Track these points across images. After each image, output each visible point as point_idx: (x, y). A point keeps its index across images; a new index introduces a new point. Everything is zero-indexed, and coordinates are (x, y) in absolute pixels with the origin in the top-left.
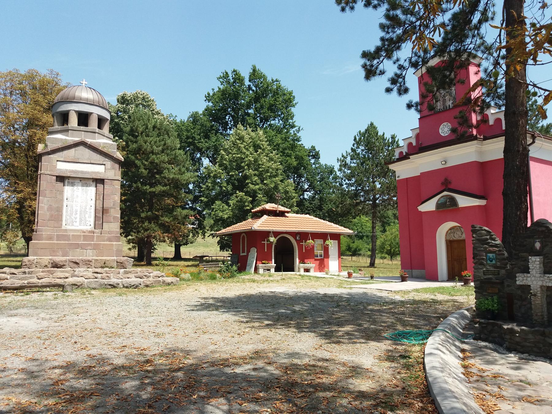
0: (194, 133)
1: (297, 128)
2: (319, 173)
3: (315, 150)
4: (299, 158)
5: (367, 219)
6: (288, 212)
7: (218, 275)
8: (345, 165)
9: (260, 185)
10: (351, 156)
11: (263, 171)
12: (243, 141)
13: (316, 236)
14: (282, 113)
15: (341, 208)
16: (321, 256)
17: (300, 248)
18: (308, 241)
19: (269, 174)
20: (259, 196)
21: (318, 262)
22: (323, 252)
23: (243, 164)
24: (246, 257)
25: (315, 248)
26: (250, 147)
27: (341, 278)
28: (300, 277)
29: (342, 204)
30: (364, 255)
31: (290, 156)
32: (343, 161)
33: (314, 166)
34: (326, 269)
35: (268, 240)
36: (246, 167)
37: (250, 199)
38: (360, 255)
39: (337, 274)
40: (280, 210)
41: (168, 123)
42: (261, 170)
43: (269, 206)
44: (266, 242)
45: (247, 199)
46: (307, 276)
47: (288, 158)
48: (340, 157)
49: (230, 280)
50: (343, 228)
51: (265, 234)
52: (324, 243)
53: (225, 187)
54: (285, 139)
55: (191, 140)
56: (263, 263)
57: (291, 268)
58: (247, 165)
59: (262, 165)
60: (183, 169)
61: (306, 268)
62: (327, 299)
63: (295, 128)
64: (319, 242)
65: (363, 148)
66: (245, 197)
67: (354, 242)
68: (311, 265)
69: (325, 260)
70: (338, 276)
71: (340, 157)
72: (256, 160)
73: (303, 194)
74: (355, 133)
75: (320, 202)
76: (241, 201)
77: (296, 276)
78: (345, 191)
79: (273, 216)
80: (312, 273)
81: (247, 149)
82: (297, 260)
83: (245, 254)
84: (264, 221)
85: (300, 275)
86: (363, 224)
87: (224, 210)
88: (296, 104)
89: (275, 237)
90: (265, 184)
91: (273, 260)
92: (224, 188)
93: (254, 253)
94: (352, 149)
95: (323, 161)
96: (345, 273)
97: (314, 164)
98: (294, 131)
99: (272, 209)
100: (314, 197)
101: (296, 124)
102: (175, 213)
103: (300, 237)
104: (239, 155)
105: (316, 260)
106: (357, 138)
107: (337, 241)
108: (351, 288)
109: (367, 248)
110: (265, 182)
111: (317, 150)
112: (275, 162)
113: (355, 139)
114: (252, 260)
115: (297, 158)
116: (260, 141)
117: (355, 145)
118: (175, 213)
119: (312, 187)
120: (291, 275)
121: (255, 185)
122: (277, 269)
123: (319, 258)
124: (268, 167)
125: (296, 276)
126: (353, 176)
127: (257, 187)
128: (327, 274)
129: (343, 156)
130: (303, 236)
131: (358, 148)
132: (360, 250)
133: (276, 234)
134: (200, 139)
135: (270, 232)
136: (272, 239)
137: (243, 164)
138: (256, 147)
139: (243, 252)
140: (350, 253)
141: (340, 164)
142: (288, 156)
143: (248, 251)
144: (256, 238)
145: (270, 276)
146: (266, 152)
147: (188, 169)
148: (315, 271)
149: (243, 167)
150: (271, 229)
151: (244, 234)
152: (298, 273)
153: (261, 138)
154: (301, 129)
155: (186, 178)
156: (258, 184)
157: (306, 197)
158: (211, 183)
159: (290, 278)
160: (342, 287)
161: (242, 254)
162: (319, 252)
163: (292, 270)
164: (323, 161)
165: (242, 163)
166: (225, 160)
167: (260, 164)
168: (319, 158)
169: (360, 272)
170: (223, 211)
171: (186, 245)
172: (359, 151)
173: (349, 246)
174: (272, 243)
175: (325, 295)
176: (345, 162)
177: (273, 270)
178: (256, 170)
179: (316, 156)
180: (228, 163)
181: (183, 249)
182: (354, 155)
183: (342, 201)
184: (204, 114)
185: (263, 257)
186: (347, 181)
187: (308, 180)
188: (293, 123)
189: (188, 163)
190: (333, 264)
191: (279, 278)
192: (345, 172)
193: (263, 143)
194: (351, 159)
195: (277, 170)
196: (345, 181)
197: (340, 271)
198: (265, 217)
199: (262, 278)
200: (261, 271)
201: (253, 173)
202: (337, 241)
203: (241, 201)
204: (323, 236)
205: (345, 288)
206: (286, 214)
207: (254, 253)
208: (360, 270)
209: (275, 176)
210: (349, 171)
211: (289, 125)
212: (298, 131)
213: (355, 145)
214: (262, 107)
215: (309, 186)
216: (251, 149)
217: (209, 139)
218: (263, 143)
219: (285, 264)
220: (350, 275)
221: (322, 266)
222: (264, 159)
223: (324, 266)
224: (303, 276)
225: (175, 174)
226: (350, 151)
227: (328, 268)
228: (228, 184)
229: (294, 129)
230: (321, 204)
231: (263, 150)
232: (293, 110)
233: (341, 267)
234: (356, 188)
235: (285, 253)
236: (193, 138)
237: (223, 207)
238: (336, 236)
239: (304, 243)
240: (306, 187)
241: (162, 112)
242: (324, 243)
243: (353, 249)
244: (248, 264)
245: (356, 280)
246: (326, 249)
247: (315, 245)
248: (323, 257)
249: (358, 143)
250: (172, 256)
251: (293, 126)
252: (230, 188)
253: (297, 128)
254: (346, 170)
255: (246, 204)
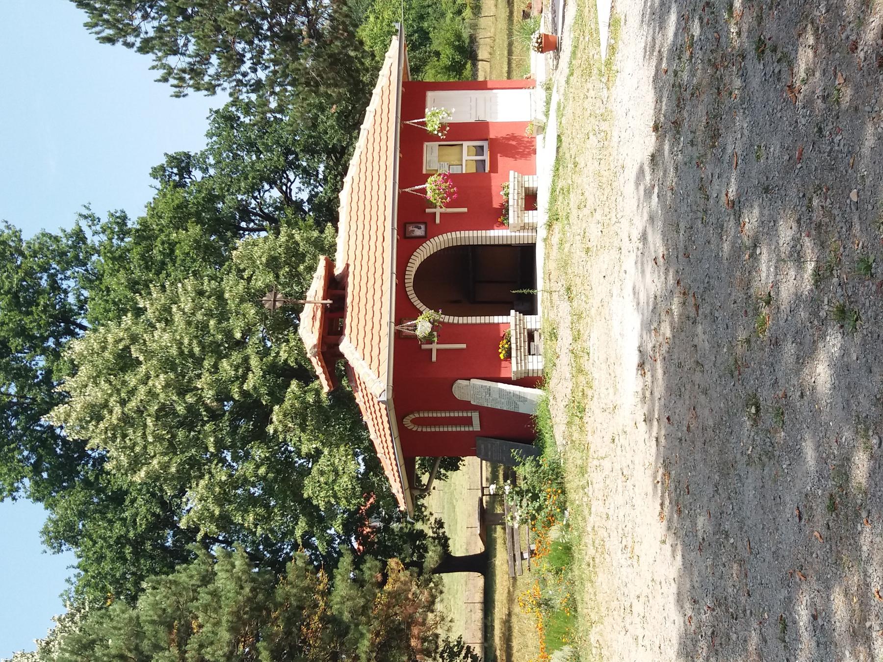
0: (105, 539)
1: (84, 224)
2: (236, 156)
3: (162, 168)
4: (181, 216)
5: (372, 19)
6: (330, 265)
7: (554, 533)
8: (195, 72)
9: (249, 351)
10: (166, 55)
11: (200, 343)
12: (105, 405)
13: (410, 169)
14: (45, 269)
15: (329, 86)
16: (480, 150)
17: (452, 223)
18: (429, 194)
19: (212, 323)
20: (283, 355)
21: (502, 161)
22: (466, 144)
23: (180, 409)
24: (486, 413)
25: (455, 170)
26: (124, 383)
27: (560, 78)
28: (557, 226)
29: (317, 85)
30: (474, 26)
31: (172, 245)
32: (182, 79)
33: (212, 171)
34: (527, 132)
35: (428, 340)
36: (190, 399)
37: (294, 385)
38: (473, 39)
39: (539, 93)
40: (321, 293)
41: (77, 618)
42: (197, 350)
43: (309, 331)
44: (435, 347)
45: (297, 398)
46: (553, 200)
47: (177, 252)
48: (167, 89)
49: (572, 482)
50: (384, 73)
51: (405, 348)
52: (435, 138)
53: (258, 467)
54: (120, 259)
55: (128, 550)
56: (509, 356)
57: (525, 254)
58: (182, 393)
59: (180, 344)
60: (204, 597)
61: (522, 203)
62: (697, 116)
63: (85, 228)
64: (432, 157)
65: (138, 15)
66: (287, 404)
67: (437, 54)
68: (510, 184)
69: (492, 135)
70: (548, 89)
71: (167, 89)
72: (168, 364)
73: (298, 205)
74: (90, 38)
75: (318, 152)
76: (300, 416)
77: (555, 240)
78: (275, 72)
79: (343, 316)
80: (541, 181)
81: (132, 392)
82: (497, 235)
83: (475, 416)
84: (358, 354)
85: (550, 226)
86: (386, 29)
87: (332, 476)
88: (8, 227)
89: (417, 313)
90: (244, 336)
91: (497, 319)
92: (262, 471)
93: (473, 389)
94: (141, 50)
95: (195, 139)
96: (538, 64)
97: (205, 170)
98: (96, 233)
99: (317, 324)
100: (305, 171)
101: (70, 228)
102: (346, 616)
103: (417, 224)
104: (149, 422)
105: (494, 168)
106: (109, 32)
107: (430, 95)
108: (614, 24)
109: (453, 19)
110: (238, 335)
111: (163, 161)
112: (175, 300)
113: (110, 40)
114: (495, 395)
115: (179, 223)
116: (104, 349)
117: (130, 39)
118: (346, 616)
119: (275, 177)
120: (547, 257)
121: (248, 369)
122: (529, 306)
123: (486, 157)
124: (189, 323)
125: (555, 240)
126: (227, 46)
127: (254, 362)
128: (542, 129)
129: (165, 80)
130: (411, 213)
131: (136, 31)
132: (459, 37)
133: (404, 311)
134: (124, 520)
135: (398, 335)
136: (423, 326)
137: (180, 409)
138: (125, 362)
139: (468, 421)
140: (469, 66)
141: (190, 91)
142: (172, 251)
143: (466, 406)
144: (417, 377)
145: (554, 335)
146: (138, 329)
147: (207, 578)
148: (532, 171)
149: (190, 408)
150: (385, 330)
151: (407, 422)
152: (542, 233)
153: (96, 346)
154: (85, 212)
155: (231, 586)
156: (246, 359)
157: (305, 196)
158: (246, 511)
159: (564, 265)
160: (608, 63)
161: (476, 427)
162: (466, 158)
163: (527, 252)
164: (195, 139)
165: (175, 414)
166: (165, 467)
167: (181, 353)
168: (188, 156)
169: (534, 13)
170: (337, 474)
171: (447, 539)
172: (149, 28)
173: (448, 69)
174: (436, 326)
175: (668, 127)
176: (184, 71)
177: (531, 322)
178: (198, 362)
179: (183, 163)
180: (177, 459)
181: (458, 549)
182: (161, 44)
183: (308, 84)
184: (51, 506)
185: (487, 356)
186: (245, 67)
187: (254, 188)
188: (68, 236)
189: (185, 575)
190: (504, 108)
191: (564, 307)
192: (218, 76)
193: (110, 339)
194: (175, 53)
195: (201, 293)
196: (245, 75)
197: (527, 84)
198: (346, 347)
199: (565, 360)
200: (535, 364)
201: (206, 377)
202: (430, 95)
203: (300, 416)
204: (411, 140)
205: (612, 49)
206: (338, 271)
207: (473, 389)
208: (526, 15)
209: (220, 296)
210: (214, 59)
211: (74, 247)
212: (92, 219)
213: (130, 39)
214: (22, 332)
215: (272, 183)
216: (132, 380)
217: (127, 492)
218: (110, 339)
219: (508, 278)
220: (549, 45)
221: (514, 146)
222: (162, 338)
223: (513, 137)
224: (553, 219)
225: (217, 624)
226: (151, 56)
227: (523, 125)
228: (247, 456)
229: (88, 233)
230: (329, 152)
231: (134, 339)
232: (28, 235)
233: (514, 78)
234: (266, 38)
235: (475, 277)
236: (121, 541)
237: (322, 473)
238: (412, 100)
239: (438, 211)
240: (276, 193)
241: (45, 636)
242: (435, 138)
243: (458, 58)
244: (511, 408)
245: (569, 20)
246: (458, 132)
247: (445, 170)
248: (485, 144)
249: (119, 33)
250: (477, 580)
251: (79, 236)
252: (259, 452)
253: (84, 224)
254: (212, 71)
255: (310, 399)
